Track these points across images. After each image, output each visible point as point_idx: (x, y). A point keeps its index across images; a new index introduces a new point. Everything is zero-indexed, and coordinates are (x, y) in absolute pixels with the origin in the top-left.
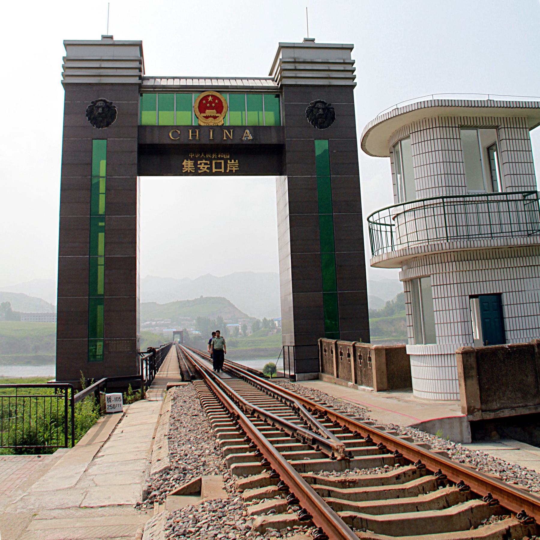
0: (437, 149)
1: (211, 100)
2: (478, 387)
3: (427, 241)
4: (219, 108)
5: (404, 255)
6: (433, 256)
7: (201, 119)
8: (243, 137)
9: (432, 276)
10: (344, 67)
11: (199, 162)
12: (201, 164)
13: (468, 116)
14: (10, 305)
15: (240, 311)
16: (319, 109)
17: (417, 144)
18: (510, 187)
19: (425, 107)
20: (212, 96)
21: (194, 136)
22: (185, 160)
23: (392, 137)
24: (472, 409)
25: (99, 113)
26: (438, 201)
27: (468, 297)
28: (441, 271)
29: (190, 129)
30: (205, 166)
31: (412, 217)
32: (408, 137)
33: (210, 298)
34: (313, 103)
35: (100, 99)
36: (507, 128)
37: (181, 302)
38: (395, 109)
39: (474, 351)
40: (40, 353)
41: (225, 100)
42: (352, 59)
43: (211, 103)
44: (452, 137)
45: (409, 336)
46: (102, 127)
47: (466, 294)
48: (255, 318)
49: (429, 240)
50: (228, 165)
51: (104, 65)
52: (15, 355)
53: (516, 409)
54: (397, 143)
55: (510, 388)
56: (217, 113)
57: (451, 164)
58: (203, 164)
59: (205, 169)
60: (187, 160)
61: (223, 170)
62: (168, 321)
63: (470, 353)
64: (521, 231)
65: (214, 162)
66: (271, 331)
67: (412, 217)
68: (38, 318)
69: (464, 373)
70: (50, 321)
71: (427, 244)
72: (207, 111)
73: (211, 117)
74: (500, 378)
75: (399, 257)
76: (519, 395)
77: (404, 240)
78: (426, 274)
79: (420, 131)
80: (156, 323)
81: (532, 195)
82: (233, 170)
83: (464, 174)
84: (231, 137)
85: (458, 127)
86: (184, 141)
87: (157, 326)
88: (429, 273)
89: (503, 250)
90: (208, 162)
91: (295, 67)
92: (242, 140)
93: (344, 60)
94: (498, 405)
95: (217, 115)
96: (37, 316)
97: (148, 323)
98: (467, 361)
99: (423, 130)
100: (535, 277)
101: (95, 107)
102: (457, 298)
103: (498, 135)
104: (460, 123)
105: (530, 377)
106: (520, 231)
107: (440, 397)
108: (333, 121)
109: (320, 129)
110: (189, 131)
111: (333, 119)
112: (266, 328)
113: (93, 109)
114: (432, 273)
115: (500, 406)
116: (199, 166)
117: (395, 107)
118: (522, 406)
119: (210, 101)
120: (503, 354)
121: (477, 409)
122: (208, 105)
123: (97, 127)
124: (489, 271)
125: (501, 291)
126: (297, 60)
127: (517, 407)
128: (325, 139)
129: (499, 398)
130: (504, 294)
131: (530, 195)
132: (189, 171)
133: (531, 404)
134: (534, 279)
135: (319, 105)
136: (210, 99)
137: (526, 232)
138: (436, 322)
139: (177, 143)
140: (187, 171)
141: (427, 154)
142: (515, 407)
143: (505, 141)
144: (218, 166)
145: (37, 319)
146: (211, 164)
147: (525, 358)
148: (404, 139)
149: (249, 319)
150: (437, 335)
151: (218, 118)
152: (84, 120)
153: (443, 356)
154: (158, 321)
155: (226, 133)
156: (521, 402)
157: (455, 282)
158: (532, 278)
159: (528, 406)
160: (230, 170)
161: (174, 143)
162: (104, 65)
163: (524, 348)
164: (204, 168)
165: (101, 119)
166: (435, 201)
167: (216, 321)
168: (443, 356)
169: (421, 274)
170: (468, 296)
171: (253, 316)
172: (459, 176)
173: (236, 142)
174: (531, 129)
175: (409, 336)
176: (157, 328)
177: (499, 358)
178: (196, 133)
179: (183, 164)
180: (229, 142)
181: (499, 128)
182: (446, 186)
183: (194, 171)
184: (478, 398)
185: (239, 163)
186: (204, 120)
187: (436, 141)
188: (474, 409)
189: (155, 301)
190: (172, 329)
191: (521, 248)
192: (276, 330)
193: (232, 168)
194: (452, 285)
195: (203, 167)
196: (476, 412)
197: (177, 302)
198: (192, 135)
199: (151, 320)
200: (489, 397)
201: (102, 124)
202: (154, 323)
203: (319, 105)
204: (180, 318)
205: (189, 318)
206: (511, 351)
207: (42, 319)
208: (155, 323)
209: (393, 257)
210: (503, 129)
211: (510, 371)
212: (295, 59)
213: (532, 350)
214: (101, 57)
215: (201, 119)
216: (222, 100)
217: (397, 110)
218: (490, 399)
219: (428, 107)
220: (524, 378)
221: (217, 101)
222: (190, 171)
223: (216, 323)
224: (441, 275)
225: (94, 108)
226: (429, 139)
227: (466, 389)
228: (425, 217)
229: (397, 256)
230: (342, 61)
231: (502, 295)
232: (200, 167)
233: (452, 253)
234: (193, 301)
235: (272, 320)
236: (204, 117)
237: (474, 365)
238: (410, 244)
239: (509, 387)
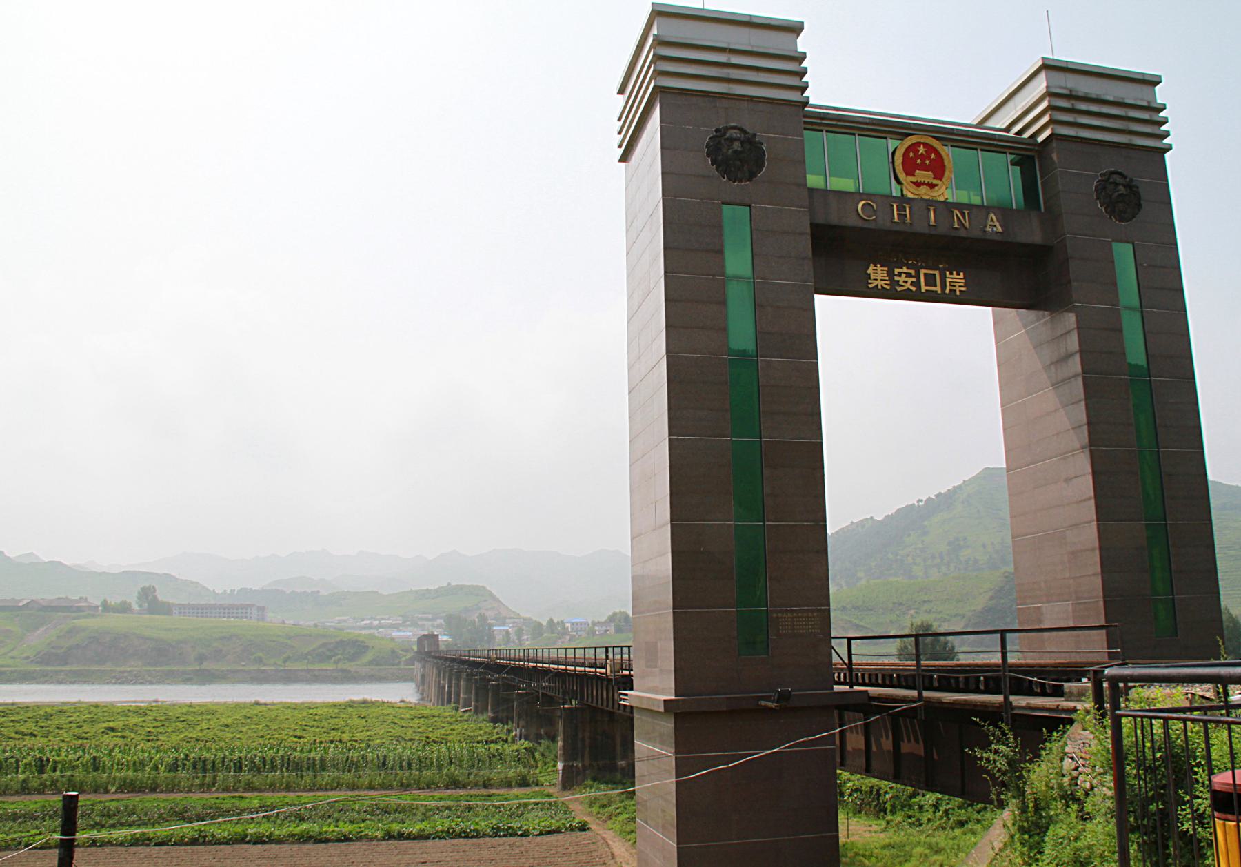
1: (924, 153)
4: (938, 169)
7: (908, 187)
8: (986, 226)
10: (1151, 116)
11: (896, 271)
12: (900, 274)
14: (155, 590)
15: (507, 608)
16: (1117, 184)
20: (925, 145)
21: (902, 216)
22: (872, 265)
25: (735, 152)
29: (895, 203)
30: (906, 279)
33: (461, 587)
34: (1104, 174)
35: (732, 124)
37: (417, 592)
40: (206, 665)
41: (948, 155)
42: (1159, 101)
43: (923, 157)
46: (740, 181)
48: (531, 619)
50: (948, 280)
51: (736, 60)
52: (167, 668)
56: (934, 178)
58: (903, 275)
59: (908, 286)
60: (876, 266)
61: (938, 289)
62: (397, 620)
65: (923, 272)
66: (560, 638)
68: (200, 611)
70: (220, 617)
72: (917, 171)
73: (924, 184)
80: (380, 623)
82: (955, 291)
84: (967, 224)
86: (883, 223)
87: (382, 628)
90: (912, 272)
91: (1073, 105)
92: (985, 231)
93: (1149, 102)
95: (935, 182)
96: (198, 609)
97: (368, 622)
101: (725, 140)
108: (1139, 210)
109: (1120, 221)
110: (892, 206)
111: (1139, 206)
112: (552, 633)
113: (719, 142)
116: (896, 278)
119: (922, 154)
122: (919, 161)
123: (729, 179)
126: (1074, 93)
128: (1128, 242)
132: (880, 287)
135: (1118, 179)
136: (922, 150)
139: (872, 226)
140: (877, 286)
144: (930, 280)
145: (198, 613)
146: (918, 276)
149: (522, 620)
151: (936, 188)
152: (706, 165)
154: (383, 619)
155: (957, 215)
160: (950, 290)
161: (866, 225)
162: (736, 60)
164: (906, 282)
165: (738, 163)
167: (477, 620)
171: (528, 616)
173: (976, 233)
176: (380, 630)
178: (905, 211)
179: (868, 272)
180: (963, 234)
183: (888, 287)
185: (965, 277)
186: (913, 188)
189: (375, 590)
190: (404, 631)
192: (568, 637)
193: (955, 286)
195: (906, 283)
197: (411, 591)
198: (898, 214)
199: (372, 618)
201: (740, 175)
202: (376, 623)
203: (1118, 179)
204: (416, 615)
205: (430, 616)
207: (206, 613)
208: (377, 622)
212: (1071, 91)
214: (729, 44)
215: (908, 187)
216: (943, 153)
221: (933, 156)
222: (882, 286)
223: (477, 624)
225: (723, 141)
230: (1145, 104)
232: (898, 281)
234: (436, 591)
235: (562, 622)
236: (912, 182)
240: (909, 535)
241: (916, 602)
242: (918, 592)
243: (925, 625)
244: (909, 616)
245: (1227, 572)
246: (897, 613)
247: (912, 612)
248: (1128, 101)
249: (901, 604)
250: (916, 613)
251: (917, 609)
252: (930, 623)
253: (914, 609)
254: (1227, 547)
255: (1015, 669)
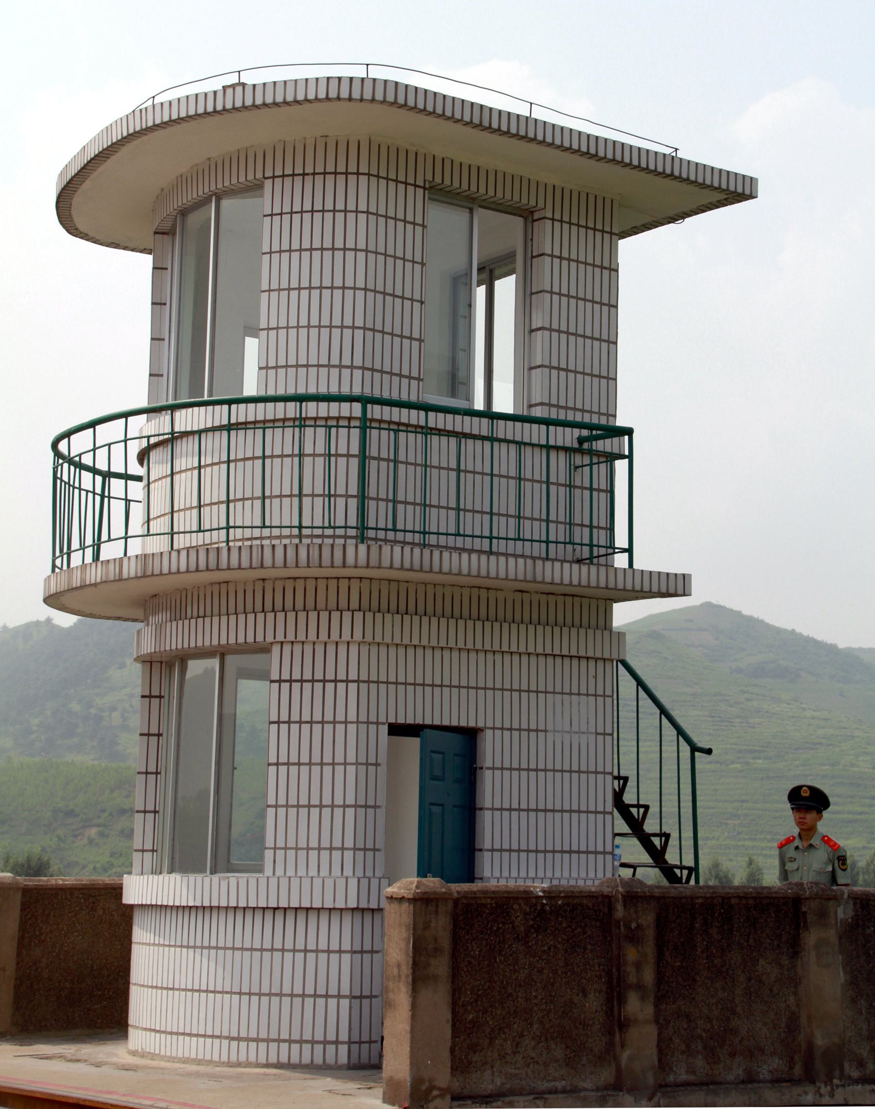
0: (350, 244)
2: (449, 1016)
3: (296, 531)
5: (207, 569)
6: (289, 585)
9: (276, 649)
13: (458, 159)
17: (287, 217)
18: (542, 404)
19: (350, 99)
23: (182, 181)
24: (424, 1088)
26: (345, 409)
27: (384, 729)
28: (312, 636)
31: (189, 459)
32: (254, 188)
36: (561, 221)
38: (233, 86)
39: (451, 894)
44: (400, 216)
45: (137, 844)
47: (382, 719)
49: (305, 532)
53: (546, 1096)
54: (204, 202)
55: (535, 1026)
57: (598, 262)
63: (437, 899)
64: (574, 544)
67: (189, 459)
69: (415, 965)
71: (297, 541)
74: (510, 990)
75: (178, 572)
76: (559, 1052)
77: (214, 517)
78: (260, 638)
79: (304, 175)
81: (608, 441)
83: (420, 340)
85: (424, 188)
88: (270, 638)
89: (501, 596)
94: (498, 1081)
98: (427, 927)
99: (314, 174)
100: (579, 694)
102: (352, 728)
103: (528, 239)
104: (429, 177)
105: (591, 996)
106: (570, 543)
107: (254, 1053)
114: (280, 637)
115: (503, 1084)
117: (233, 79)
118: (564, 1091)
120: (526, 914)
121: (440, 1089)
124: (455, 654)
125: (481, 724)
127: (550, 1092)
129: (502, 1057)
130: (489, 733)
131: (611, 437)
133: (588, 1085)
134: (575, 698)
137: (586, 549)
138: (271, 801)
141: (285, 256)
142: (544, 1092)
143: (548, 260)
147: (585, 933)
148: (231, 192)
150: (269, 842)
153: (279, 916)
156: (562, 1078)
157: (353, 676)
158: (571, 694)
159: (580, 1091)
163: (585, 901)
166: (334, 409)
168: (279, 916)
169: (232, 641)
170: (386, 727)
172: (406, 342)
174: (624, 235)
175: (137, 844)
177: (513, 927)
181: (536, 216)
182: (363, 368)
184: (446, 1054)
187: (351, 217)
188: (432, 1088)
191: (552, 599)
194: (341, 686)
196: (435, 1097)
200: (475, 1052)
206: (548, 908)
209: (165, 570)
210: (549, 223)
211: (541, 971)
213: (606, 910)
217: (239, 89)
218: (476, 1058)
219: (362, 100)
220: (576, 999)
224: (308, 649)
226: (297, 208)
227: (413, 1017)
228: (264, 457)
229: (183, 568)
231: (480, 737)
233: (355, 584)
237: (446, 942)
238: (234, 534)
239: (531, 1024)
240: (122, 666)
241: (103, 811)
242: (112, 791)
243: (33, 864)
244: (85, 841)
245: (743, 801)
246: (60, 832)
247: (93, 832)
248: (384, 1042)
249: (71, 813)
250: (102, 835)
251: (105, 826)
252: (45, 858)
253: (99, 826)
254: (751, 751)
255: (163, 1064)
